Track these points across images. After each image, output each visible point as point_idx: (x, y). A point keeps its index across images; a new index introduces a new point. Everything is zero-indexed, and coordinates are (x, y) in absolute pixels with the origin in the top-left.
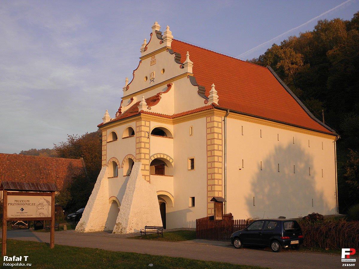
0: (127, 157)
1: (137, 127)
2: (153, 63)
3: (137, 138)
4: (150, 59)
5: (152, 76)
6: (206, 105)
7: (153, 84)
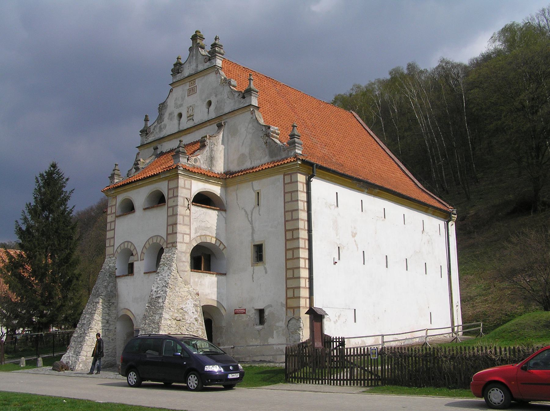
0: (151, 240)
2: (192, 91)
3: (168, 208)
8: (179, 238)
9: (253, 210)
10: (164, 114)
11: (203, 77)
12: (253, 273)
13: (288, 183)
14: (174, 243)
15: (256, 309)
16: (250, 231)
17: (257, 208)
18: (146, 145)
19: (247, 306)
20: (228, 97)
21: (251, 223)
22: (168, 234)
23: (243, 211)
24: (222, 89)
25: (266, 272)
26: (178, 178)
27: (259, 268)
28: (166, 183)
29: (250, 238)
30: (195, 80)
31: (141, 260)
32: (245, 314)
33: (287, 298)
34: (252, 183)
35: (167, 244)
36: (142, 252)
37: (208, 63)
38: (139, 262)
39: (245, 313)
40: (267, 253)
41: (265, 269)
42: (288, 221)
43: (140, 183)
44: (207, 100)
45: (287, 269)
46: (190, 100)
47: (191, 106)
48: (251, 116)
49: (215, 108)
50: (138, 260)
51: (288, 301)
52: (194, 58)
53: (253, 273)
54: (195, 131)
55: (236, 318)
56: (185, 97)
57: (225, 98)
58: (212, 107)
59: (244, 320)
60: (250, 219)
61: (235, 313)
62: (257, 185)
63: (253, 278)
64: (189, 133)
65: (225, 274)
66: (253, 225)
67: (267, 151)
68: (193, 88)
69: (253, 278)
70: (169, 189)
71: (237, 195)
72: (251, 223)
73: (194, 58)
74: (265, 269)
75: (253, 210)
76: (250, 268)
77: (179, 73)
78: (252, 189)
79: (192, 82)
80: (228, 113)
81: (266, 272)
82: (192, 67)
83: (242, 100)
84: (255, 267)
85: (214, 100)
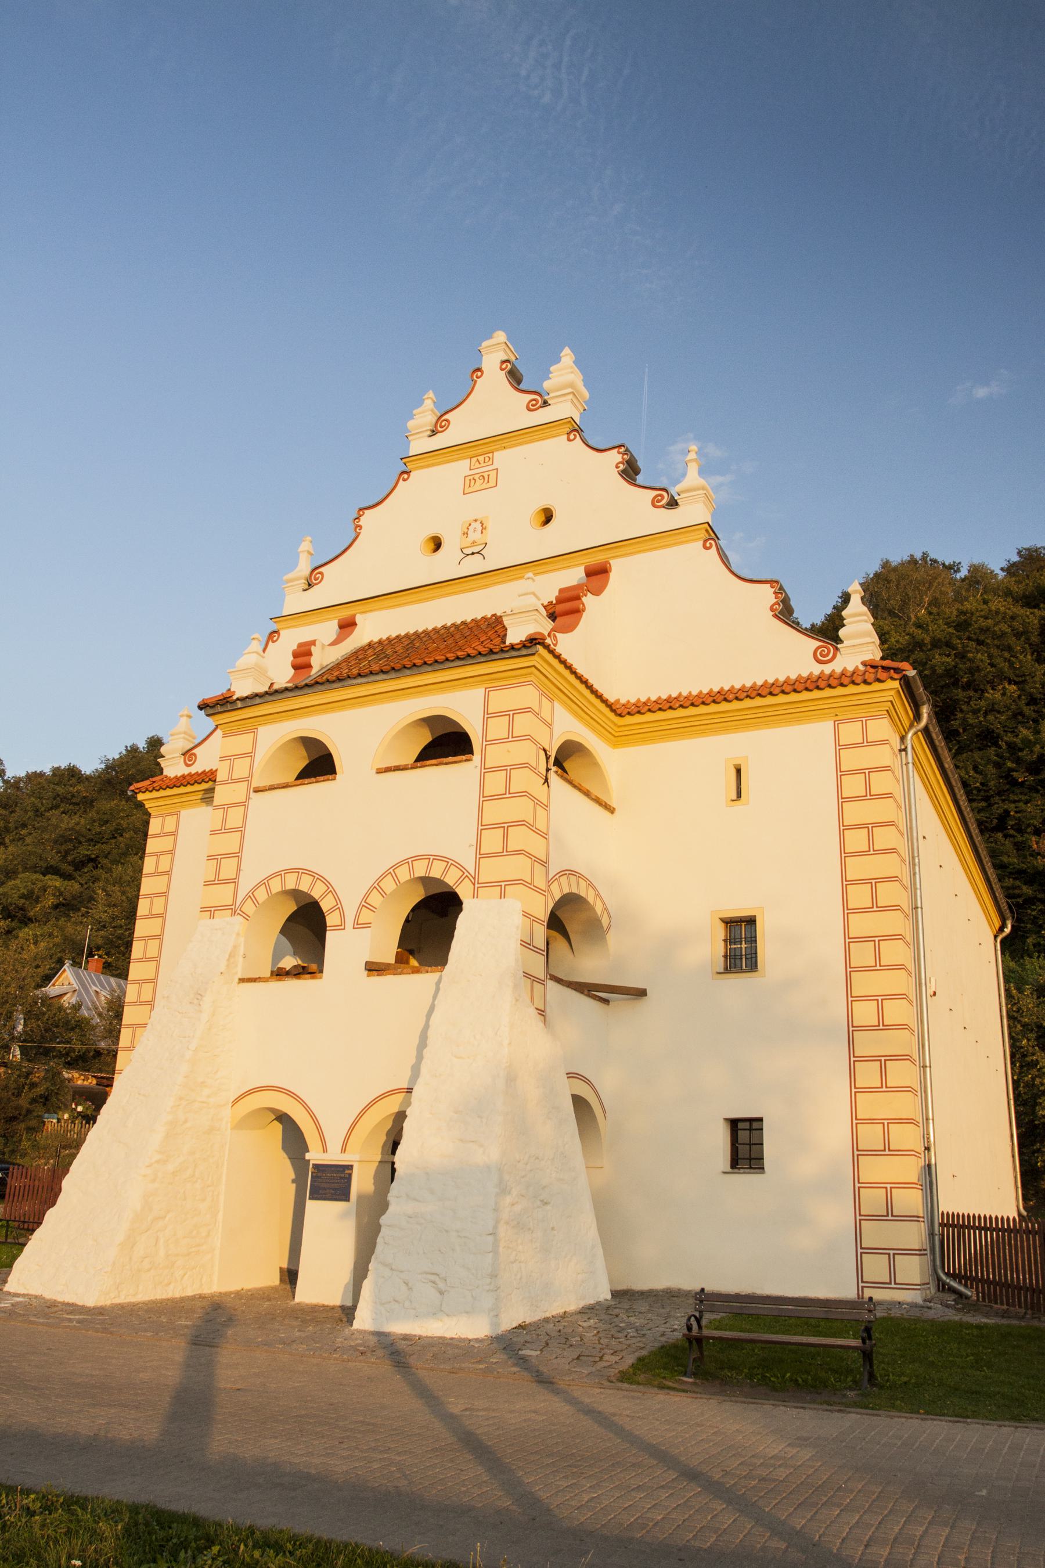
1: (488, 715)
3: (486, 770)
4: (461, 467)
5: (474, 536)
6: (827, 669)
7: (475, 565)
15: (726, 1119)
22: (480, 855)
30: (490, 455)
68: (486, 475)
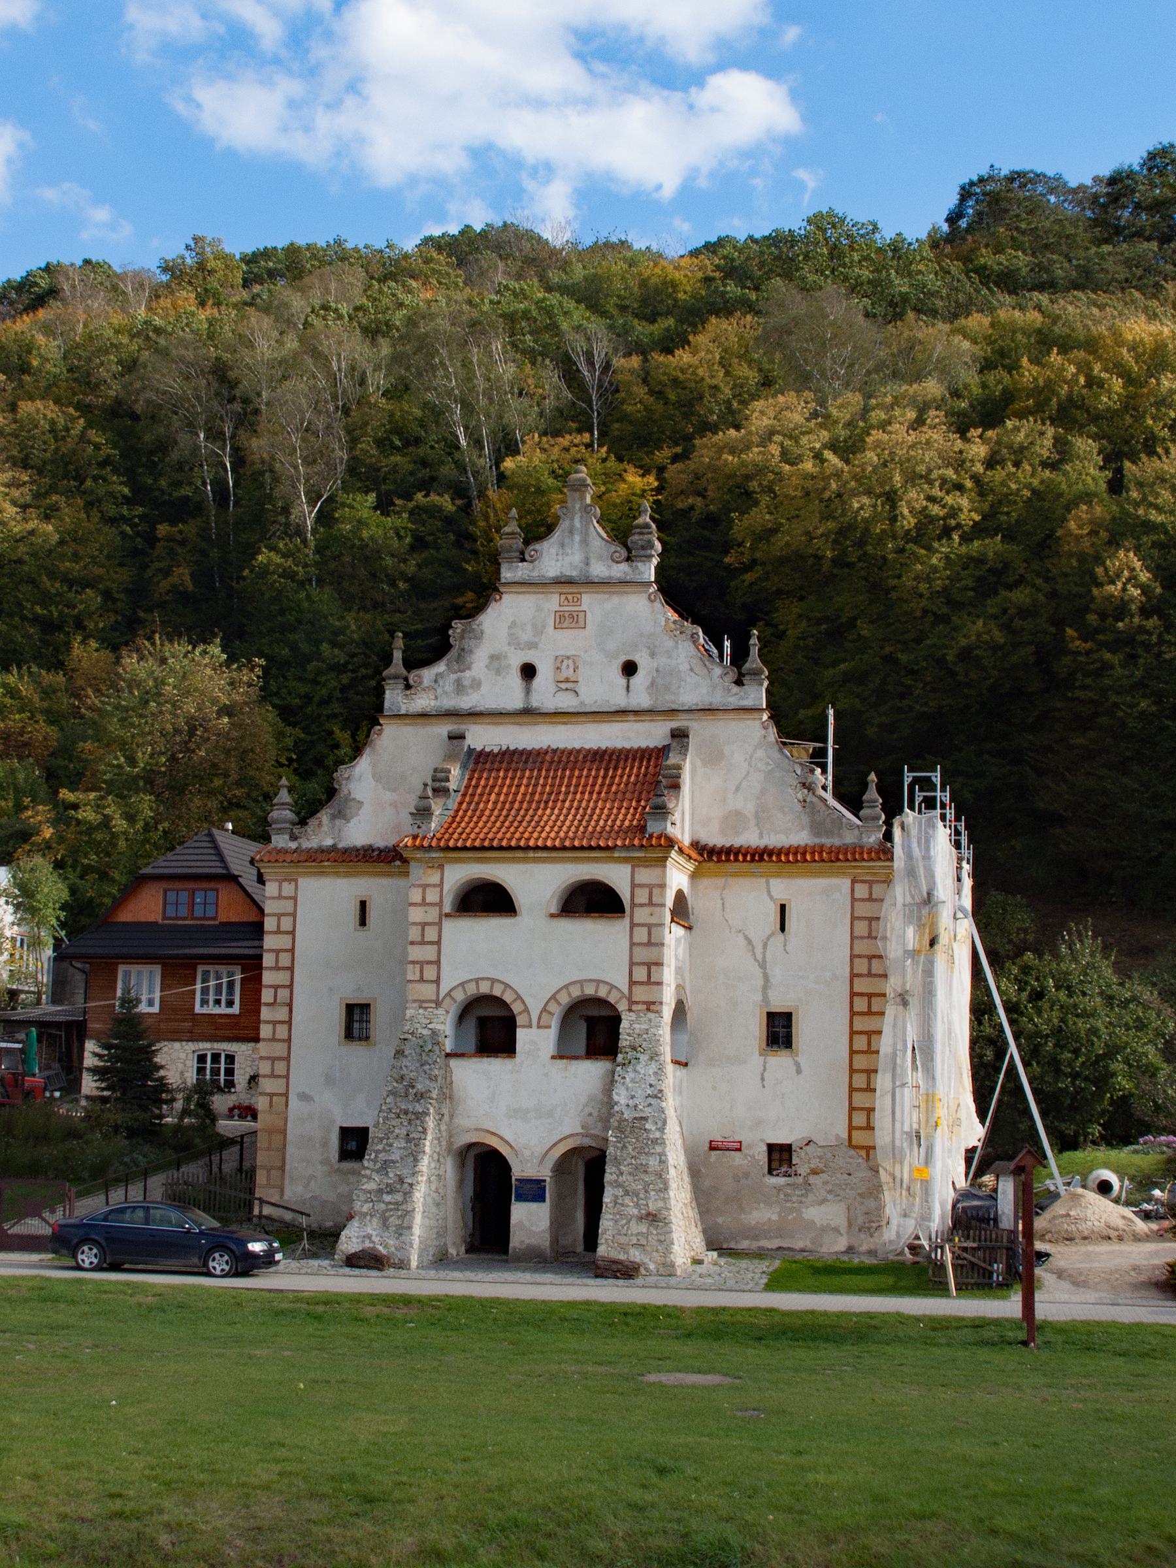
2: (569, 620)
3: (633, 925)
8: (55, 877)
9: (768, 938)
10: (471, 651)
11: (607, 596)
12: (765, 1070)
13: (863, 900)
14: (654, 1003)
16: (760, 982)
17: (781, 936)
18: (433, 720)
19: (745, 1137)
20: (692, 670)
21: (763, 965)
23: (741, 939)
24: (671, 643)
25: (799, 1071)
26: (665, 866)
27: (780, 1061)
28: (626, 869)
29: (758, 997)
31: (539, 1027)
32: (737, 1154)
33: (851, 1128)
34: (768, 883)
35: (632, 1002)
36: (544, 1009)
37: (624, 567)
38: (534, 1030)
39: (739, 1150)
40: (802, 1031)
41: (797, 1064)
42: (859, 975)
43: (545, 854)
44: (624, 658)
45: (852, 1071)
46: (567, 641)
47: (568, 658)
48: (763, 732)
49: (648, 683)
50: (530, 1026)
51: (854, 1133)
52: (577, 538)
53: (765, 1070)
54: (585, 722)
55: (713, 1159)
56: (544, 627)
57: (682, 668)
58: (638, 680)
59: (736, 1163)
60: (759, 957)
61: (712, 1148)
62: (782, 887)
63: (763, 1079)
64: (564, 723)
65: (686, 1065)
66: (768, 971)
67: (805, 820)
69: (763, 1079)
70: (634, 886)
71: (722, 899)
72: (763, 965)
73: (577, 538)
74: (797, 1064)
75: (768, 938)
76: (756, 1060)
77: (523, 560)
78: (765, 895)
79: (570, 597)
80: (690, 711)
81: (799, 1071)
82: (568, 559)
83: (735, 689)
84: (769, 1058)
85: (641, 660)
